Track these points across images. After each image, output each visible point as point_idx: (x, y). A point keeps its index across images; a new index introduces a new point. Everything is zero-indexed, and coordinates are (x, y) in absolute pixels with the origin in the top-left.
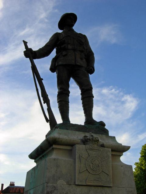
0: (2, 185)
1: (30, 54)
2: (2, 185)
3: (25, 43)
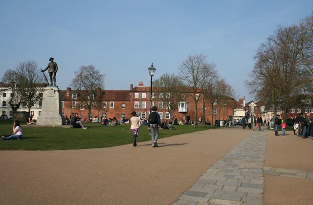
1: (42, 71)
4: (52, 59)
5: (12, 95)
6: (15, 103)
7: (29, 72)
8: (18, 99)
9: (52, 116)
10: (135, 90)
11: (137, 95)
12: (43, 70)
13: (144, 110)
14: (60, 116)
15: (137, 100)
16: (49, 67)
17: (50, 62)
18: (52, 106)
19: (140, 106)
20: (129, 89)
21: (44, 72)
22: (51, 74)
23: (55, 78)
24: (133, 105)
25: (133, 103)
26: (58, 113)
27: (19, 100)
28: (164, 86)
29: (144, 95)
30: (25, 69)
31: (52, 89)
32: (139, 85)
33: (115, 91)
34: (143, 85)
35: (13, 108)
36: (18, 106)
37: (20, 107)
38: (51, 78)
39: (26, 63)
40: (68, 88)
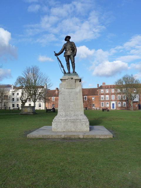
0: (98, 85)
1: (57, 55)
2: (98, 85)
3: (55, 52)
4: (68, 38)
5: (22, 94)
6: (24, 99)
7: (33, 74)
8: (26, 96)
9: (74, 118)
10: (101, 87)
11: (102, 90)
12: (57, 52)
13: (107, 101)
14: (85, 117)
15: (102, 94)
16: (65, 48)
17: (66, 42)
18: (72, 103)
19: (105, 98)
20: (96, 87)
21: (59, 56)
22: (68, 58)
23: (73, 63)
24: (100, 98)
25: (100, 97)
26: (83, 113)
27: (27, 97)
28: (124, 83)
29: (107, 91)
30: (30, 73)
31: (72, 79)
32: (103, 84)
33: (87, 89)
34: (105, 84)
35: (22, 102)
36: (26, 101)
37: (27, 101)
38: (68, 64)
39: (31, 67)
40: (56, 88)
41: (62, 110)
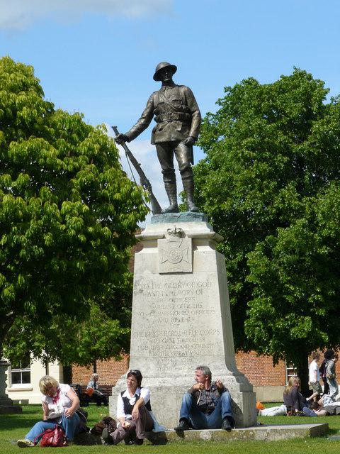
41: (146, 353)
